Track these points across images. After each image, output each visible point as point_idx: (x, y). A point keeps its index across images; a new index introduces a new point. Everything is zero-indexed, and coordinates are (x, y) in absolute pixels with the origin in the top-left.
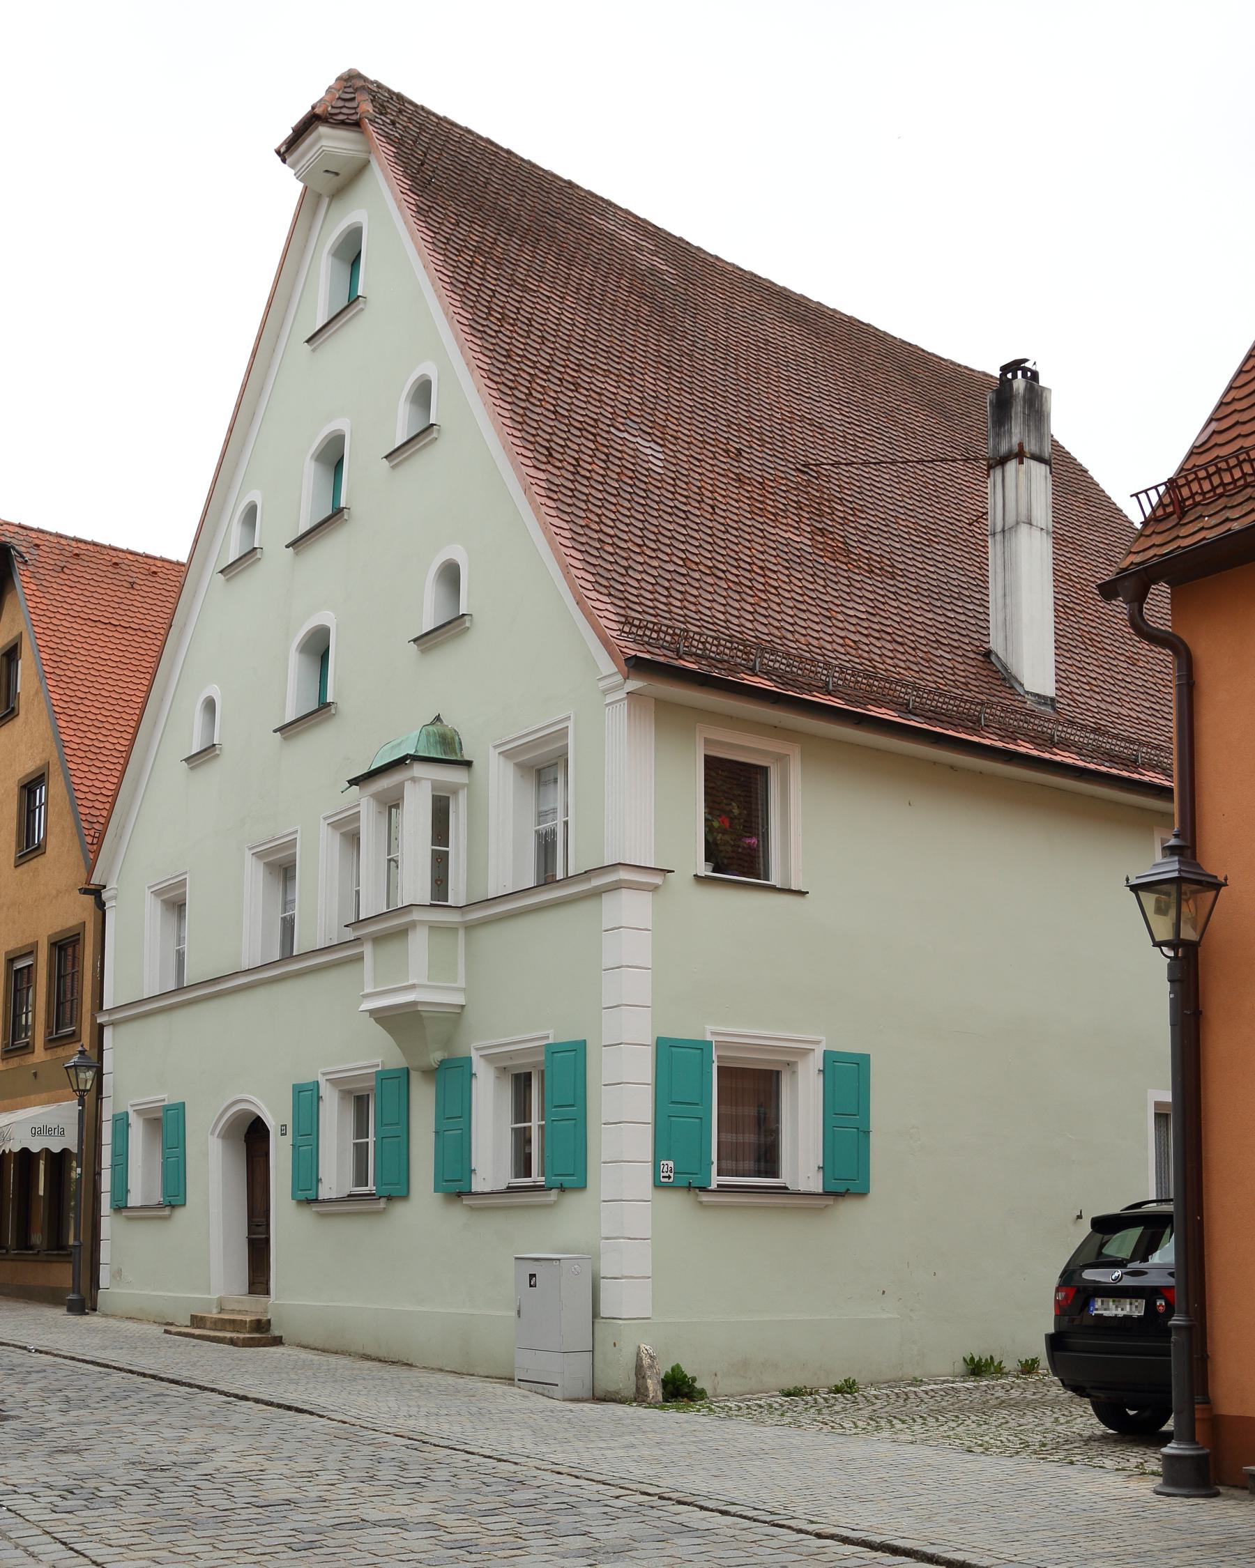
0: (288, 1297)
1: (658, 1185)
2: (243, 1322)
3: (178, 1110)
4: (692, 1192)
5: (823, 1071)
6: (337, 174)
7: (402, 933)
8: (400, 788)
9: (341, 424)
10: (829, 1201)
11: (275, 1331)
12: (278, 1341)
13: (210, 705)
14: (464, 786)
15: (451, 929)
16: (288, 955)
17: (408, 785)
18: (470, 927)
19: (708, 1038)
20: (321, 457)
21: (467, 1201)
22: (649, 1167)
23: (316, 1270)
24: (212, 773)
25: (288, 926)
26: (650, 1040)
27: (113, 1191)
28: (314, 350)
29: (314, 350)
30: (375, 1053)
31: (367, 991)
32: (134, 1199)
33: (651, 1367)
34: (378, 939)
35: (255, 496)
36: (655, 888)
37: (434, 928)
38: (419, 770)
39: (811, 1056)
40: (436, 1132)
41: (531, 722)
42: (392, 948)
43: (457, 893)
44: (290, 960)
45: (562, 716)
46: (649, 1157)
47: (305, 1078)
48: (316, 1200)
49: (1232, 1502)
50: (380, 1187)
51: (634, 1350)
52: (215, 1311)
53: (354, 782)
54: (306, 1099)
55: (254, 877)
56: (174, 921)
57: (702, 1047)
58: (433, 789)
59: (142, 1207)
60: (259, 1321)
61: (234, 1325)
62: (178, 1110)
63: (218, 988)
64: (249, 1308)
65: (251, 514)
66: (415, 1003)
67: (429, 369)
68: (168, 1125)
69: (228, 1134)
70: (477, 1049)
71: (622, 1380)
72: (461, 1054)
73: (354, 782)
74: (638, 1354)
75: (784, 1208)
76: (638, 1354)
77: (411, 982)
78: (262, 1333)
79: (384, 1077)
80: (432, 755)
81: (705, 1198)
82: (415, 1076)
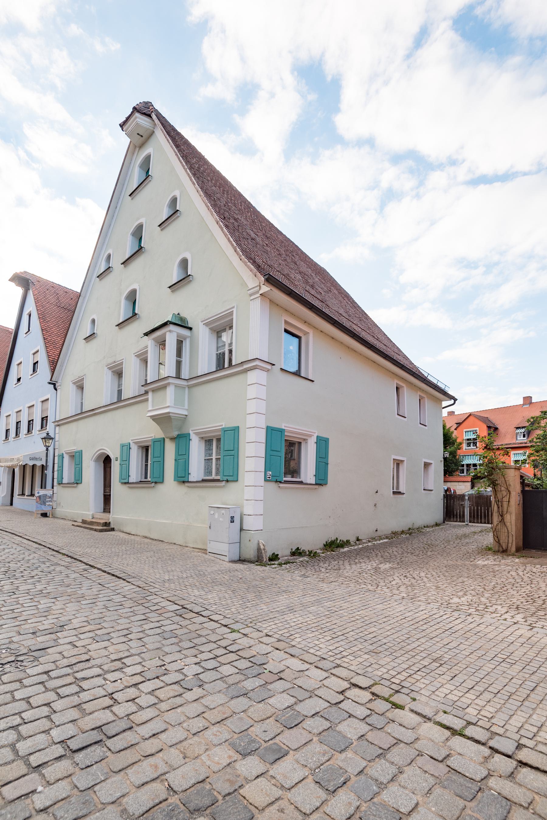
0: (116, 515)
1: (266, 480)
2: (100, 523)
3: (81, 452)
4: (277, 484)
5: (316, 443)
6: (142, 136)
7: (164, 387)
8: (165, 334)
9: (142, 220)
10: (317, 487)
11: (112, 526)
12: (113, 530)
13: (93, 321)
14: (189, 337)
15: (183, 388)
16: (119, 400)
17: (168, 334)
18: (189, 387)
19: (283, 428)
20: (134, 234)
21: (187, 484)
22: (263, 474)
23: (128, 506)
24: (94, 343)
25: (120, 392)
26: (264, 427)
27: (58, 478)
28: (132, 199)
29: (132, 199)
30: (153, 432)
31: (150, 409)
32: (65, 481)
33: (264, 549)
34: (154, 391)
35: (110, 251)
36: (268, 370)
37: (176, 386)
38: (172, 327)
39: (313, 437)
40: (175, 460)
41: (216, 310)
42: (160, 394)
43: (185, 374)
44: (120, 401)
45: (231, 306)
46: (264, 471)
47: (125, 441)
48: (128, 483)
49: (368, 566)
50: (151, 479)
51: (256, 542)
52: (91, 518)
53: (146, 334)
54: (126, 448)
55: (108, 377)
56: (79, 392)
57: (281, 431)
58: (177, 337)
59: (68, 484)
60: (106, 523)
61: (98, 524)
62: (81, 452)
63: (94, 412)
64: (103, 518)
65: (109, 256)
66: (169, 413)
67: (177, 193)
68: (76, 457)
69: (97, 460)
70: (192, 431)
71: (251, 553)
72: (184, 431)
73: (146, 334)
74: (258, 544)
75: (304, 488)
76: (258, 544)
77: (167, 405)
78: (107, 527)
79: (155, 441)
80: (177, 323)
81: (281, 485)
82: (167, 442)
